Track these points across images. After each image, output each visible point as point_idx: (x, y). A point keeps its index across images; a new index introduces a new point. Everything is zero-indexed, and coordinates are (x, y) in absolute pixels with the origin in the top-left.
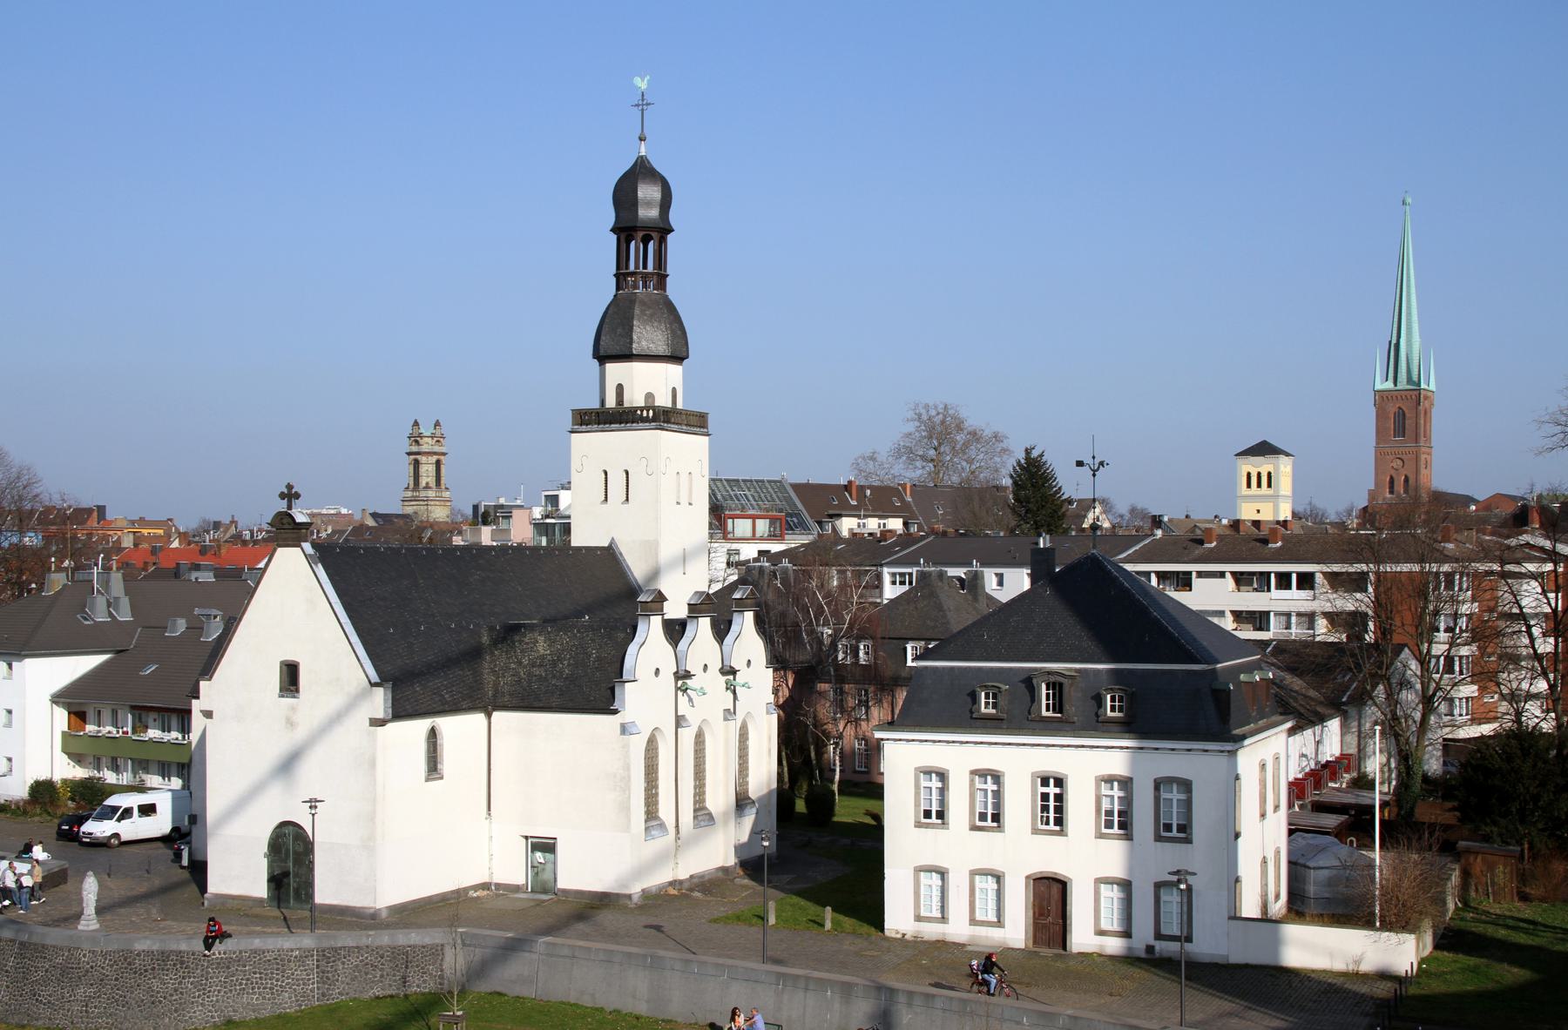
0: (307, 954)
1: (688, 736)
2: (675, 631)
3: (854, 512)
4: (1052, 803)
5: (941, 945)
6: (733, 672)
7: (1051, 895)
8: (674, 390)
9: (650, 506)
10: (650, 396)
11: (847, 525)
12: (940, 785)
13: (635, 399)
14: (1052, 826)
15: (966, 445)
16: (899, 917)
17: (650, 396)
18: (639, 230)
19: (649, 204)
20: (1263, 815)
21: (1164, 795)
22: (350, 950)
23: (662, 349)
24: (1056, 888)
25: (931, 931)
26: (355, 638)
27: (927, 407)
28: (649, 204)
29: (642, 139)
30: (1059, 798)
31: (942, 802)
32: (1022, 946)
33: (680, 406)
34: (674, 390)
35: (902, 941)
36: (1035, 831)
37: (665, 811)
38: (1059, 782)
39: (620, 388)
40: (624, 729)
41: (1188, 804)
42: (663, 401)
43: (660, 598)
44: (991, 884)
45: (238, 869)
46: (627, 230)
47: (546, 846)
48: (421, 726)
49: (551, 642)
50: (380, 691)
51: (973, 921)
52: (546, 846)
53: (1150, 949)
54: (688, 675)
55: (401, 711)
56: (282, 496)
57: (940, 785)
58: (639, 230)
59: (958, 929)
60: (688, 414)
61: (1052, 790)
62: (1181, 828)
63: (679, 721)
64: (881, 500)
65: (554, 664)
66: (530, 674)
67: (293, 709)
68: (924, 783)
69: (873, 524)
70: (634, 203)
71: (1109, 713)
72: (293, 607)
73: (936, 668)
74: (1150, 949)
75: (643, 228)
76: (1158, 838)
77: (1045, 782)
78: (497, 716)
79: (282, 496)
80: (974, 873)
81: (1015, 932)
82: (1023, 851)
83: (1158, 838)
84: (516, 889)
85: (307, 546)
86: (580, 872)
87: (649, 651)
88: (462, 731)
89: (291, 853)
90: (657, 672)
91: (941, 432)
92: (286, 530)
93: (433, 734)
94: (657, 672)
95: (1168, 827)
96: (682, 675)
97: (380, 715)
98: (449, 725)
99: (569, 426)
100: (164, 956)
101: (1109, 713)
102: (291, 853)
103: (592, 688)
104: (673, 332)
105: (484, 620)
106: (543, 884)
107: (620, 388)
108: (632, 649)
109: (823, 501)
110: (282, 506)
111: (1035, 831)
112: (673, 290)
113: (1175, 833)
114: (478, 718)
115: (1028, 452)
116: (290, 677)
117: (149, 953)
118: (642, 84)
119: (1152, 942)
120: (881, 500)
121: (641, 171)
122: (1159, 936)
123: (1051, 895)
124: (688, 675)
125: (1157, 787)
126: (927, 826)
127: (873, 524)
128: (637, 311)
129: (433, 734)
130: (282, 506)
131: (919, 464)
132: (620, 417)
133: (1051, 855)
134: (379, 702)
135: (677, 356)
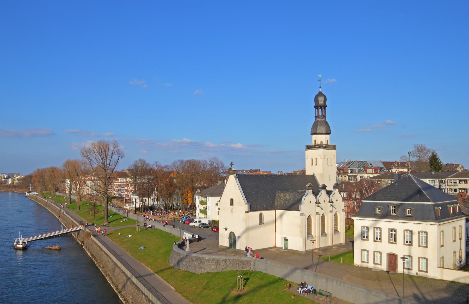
0: (223, 260)
1: (319, 217)
2: (329, 193)
3: (395, 167)
4: (393, 236)
5: (367, 269)
6: (332, 202)
7: (392, 258)
8: (327, 141)
9: (321, 165)
10: (321, 142)
11: (394, 170)
12: (426, 236)
13: (318, 143)
14: (393, 242)
15: (427, 152)
16: (357, 261)
17: (321, 142)
18: (320, 107)
19: (321, 101)
20: (454, 241)
21: (421, 235)
22: (232, 260)
23: (324, 132)
24: (394, 257)
25: (365, 265)
26: (243, 194)
27: (417, 145)
28: (321, 101)
29: (320, 87)
30: (395, 235)
31: (381, 236)
32: (386, 270)
33: (329, 144)
34: (327, 141)
35: (358, 267)
36: (389, 242)
37: (313, 233)
38: (395, 231)
39: (315, 140)
40: (301, 215)
41: (381, 233)
42: (325, 143)
43: (324, 187)
44: (424, 261)
45: (224, 241)
46: (317, 107)
47: (286, 240)
48: (258, 213)
49: (289, 195)
50: (247, 205)
51: (374, 263)
52: (286, 240)
53: (417, 274)
54: (319, 203)
55: (252, 209)
56: (231, 165)
57: (426, 236)
58: (320, 107)
59: (371, 265)
60: (330, 146)
61: (393, 233)
62: (380, 239)
63: (317, 213)
64: (403, 165)
65: (289, 200)
66: (284, 202)
67: (232, 208)
68: (406, 234)
69: (400, 170)
70: (318, 101)
71: (407, 214)
72: (232, 187)
73: (367, 203)
74: (417, 274)
75: (320, 106)
76: (375, 241)
77: (392, 231)
78: (277, 211)
79: (231, 165)
80: (419, 258)
81: (384, 267)
82: (386, 248)
83: (375, 241)
84: (281, 248)
85: (235, 175)
86: (291, 246)
87: (309, 198)
88: (268, 215)
89: (233, 239)
90: (310, 202)
91: (421, 149)
92: (231, 172)
93: (261, 215)
94: (310, 202)
95: (377, 238)
96: (318, 203)
97: (247, 210)
98: (265, 213)
99: (305, 149)
100: (197, 258)
101: (407, 214)
102: (233, 239)
103: (294, 206)
104: (327, 128)
105: (271, 190)
106: (286, 248)
107: (315, 140)
108: (304, 197)
109: (389, 165)
110: (230, 166)
111: (389, 242)
112: (327, 119)
113: (378, 240)
114: (273, 211)
115: (433, 153)
116: (232, 201)
117: (195, 257)
118: (320, 76)
119: (418, 272)
120: (403, 165)
121: (320, 94)
122: (419, 270)
123: (392, 258)
124: (319, 203)
125: (419, 233)
126: (364, 240)
127: (400, 170)
128: (319, 124)
129: (261, 215)
130: (230, 166)
131: (415, 157)
132: (316, 147)
133: (392, 249)
134: (246, 207)
135: (328, 133)
